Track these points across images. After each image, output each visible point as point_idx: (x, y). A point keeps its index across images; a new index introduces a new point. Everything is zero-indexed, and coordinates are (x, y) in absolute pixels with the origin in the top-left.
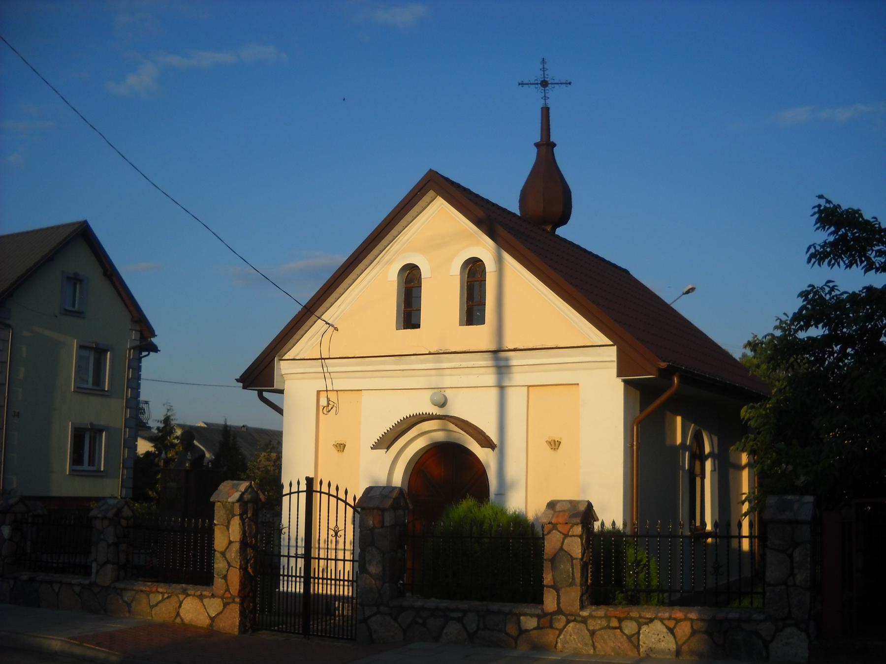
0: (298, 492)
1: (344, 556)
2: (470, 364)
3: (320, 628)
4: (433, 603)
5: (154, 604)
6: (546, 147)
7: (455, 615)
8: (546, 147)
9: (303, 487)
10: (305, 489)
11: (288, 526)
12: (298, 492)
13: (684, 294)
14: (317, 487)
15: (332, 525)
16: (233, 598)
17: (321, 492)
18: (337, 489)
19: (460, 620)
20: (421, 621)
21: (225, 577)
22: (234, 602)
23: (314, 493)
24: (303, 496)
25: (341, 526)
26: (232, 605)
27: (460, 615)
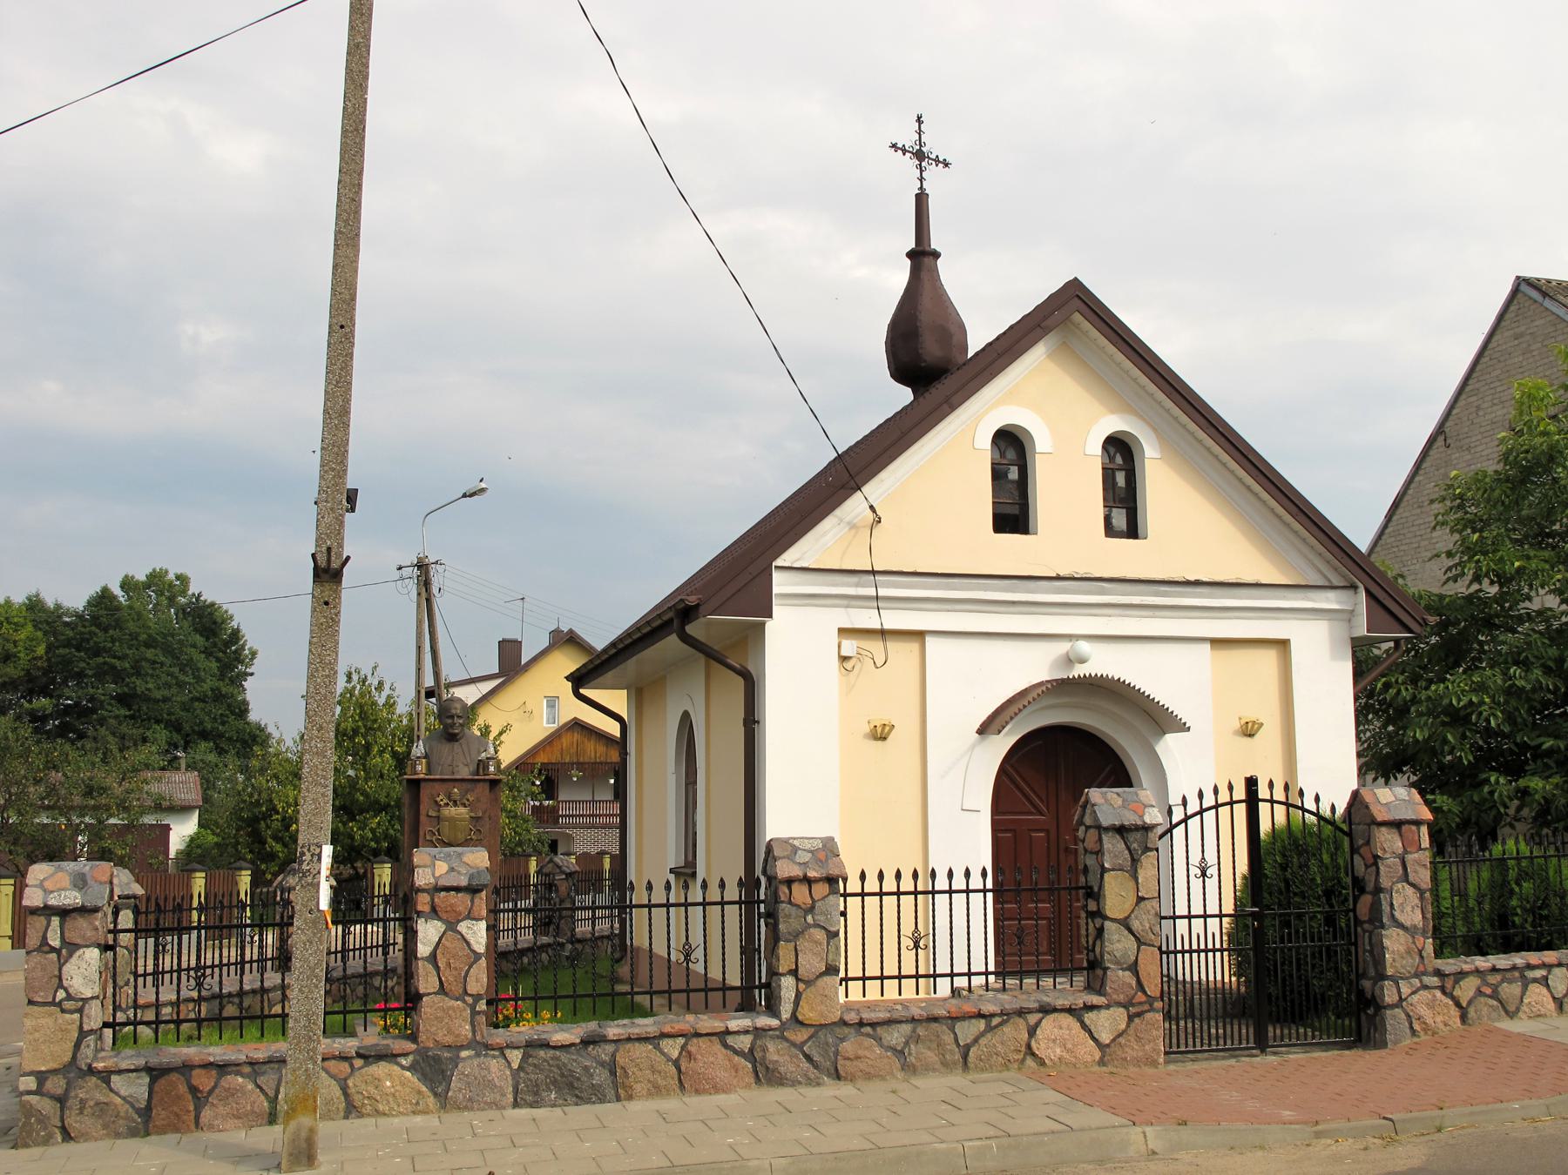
0: (1231, 803)
1: (968, 899)
2: (1136, 600)
3: (1182, 1023)
4: (1502, 961)
5: (969, 1041)
6: (922, 256)
7: (1539, 973)
8: (922, 256)
9: (1240, 794)
10: (1243, 797)
11: (1216, 862)
12: (1231, 803)
13: (465, 496)
14: (1263, 792)
15: (1195, 858)
16: (1151, 1000)
17: (1272, 801)
18: (1317, 799)
19: (1544, 981)
20: (1488, 991)
21: (1134, 968)
22: (1152, 1009)
23: (1260, 803)
24: (1241, 810)
25: (1211, 858)
26: (1148, 1016)
27: (1544, 972)
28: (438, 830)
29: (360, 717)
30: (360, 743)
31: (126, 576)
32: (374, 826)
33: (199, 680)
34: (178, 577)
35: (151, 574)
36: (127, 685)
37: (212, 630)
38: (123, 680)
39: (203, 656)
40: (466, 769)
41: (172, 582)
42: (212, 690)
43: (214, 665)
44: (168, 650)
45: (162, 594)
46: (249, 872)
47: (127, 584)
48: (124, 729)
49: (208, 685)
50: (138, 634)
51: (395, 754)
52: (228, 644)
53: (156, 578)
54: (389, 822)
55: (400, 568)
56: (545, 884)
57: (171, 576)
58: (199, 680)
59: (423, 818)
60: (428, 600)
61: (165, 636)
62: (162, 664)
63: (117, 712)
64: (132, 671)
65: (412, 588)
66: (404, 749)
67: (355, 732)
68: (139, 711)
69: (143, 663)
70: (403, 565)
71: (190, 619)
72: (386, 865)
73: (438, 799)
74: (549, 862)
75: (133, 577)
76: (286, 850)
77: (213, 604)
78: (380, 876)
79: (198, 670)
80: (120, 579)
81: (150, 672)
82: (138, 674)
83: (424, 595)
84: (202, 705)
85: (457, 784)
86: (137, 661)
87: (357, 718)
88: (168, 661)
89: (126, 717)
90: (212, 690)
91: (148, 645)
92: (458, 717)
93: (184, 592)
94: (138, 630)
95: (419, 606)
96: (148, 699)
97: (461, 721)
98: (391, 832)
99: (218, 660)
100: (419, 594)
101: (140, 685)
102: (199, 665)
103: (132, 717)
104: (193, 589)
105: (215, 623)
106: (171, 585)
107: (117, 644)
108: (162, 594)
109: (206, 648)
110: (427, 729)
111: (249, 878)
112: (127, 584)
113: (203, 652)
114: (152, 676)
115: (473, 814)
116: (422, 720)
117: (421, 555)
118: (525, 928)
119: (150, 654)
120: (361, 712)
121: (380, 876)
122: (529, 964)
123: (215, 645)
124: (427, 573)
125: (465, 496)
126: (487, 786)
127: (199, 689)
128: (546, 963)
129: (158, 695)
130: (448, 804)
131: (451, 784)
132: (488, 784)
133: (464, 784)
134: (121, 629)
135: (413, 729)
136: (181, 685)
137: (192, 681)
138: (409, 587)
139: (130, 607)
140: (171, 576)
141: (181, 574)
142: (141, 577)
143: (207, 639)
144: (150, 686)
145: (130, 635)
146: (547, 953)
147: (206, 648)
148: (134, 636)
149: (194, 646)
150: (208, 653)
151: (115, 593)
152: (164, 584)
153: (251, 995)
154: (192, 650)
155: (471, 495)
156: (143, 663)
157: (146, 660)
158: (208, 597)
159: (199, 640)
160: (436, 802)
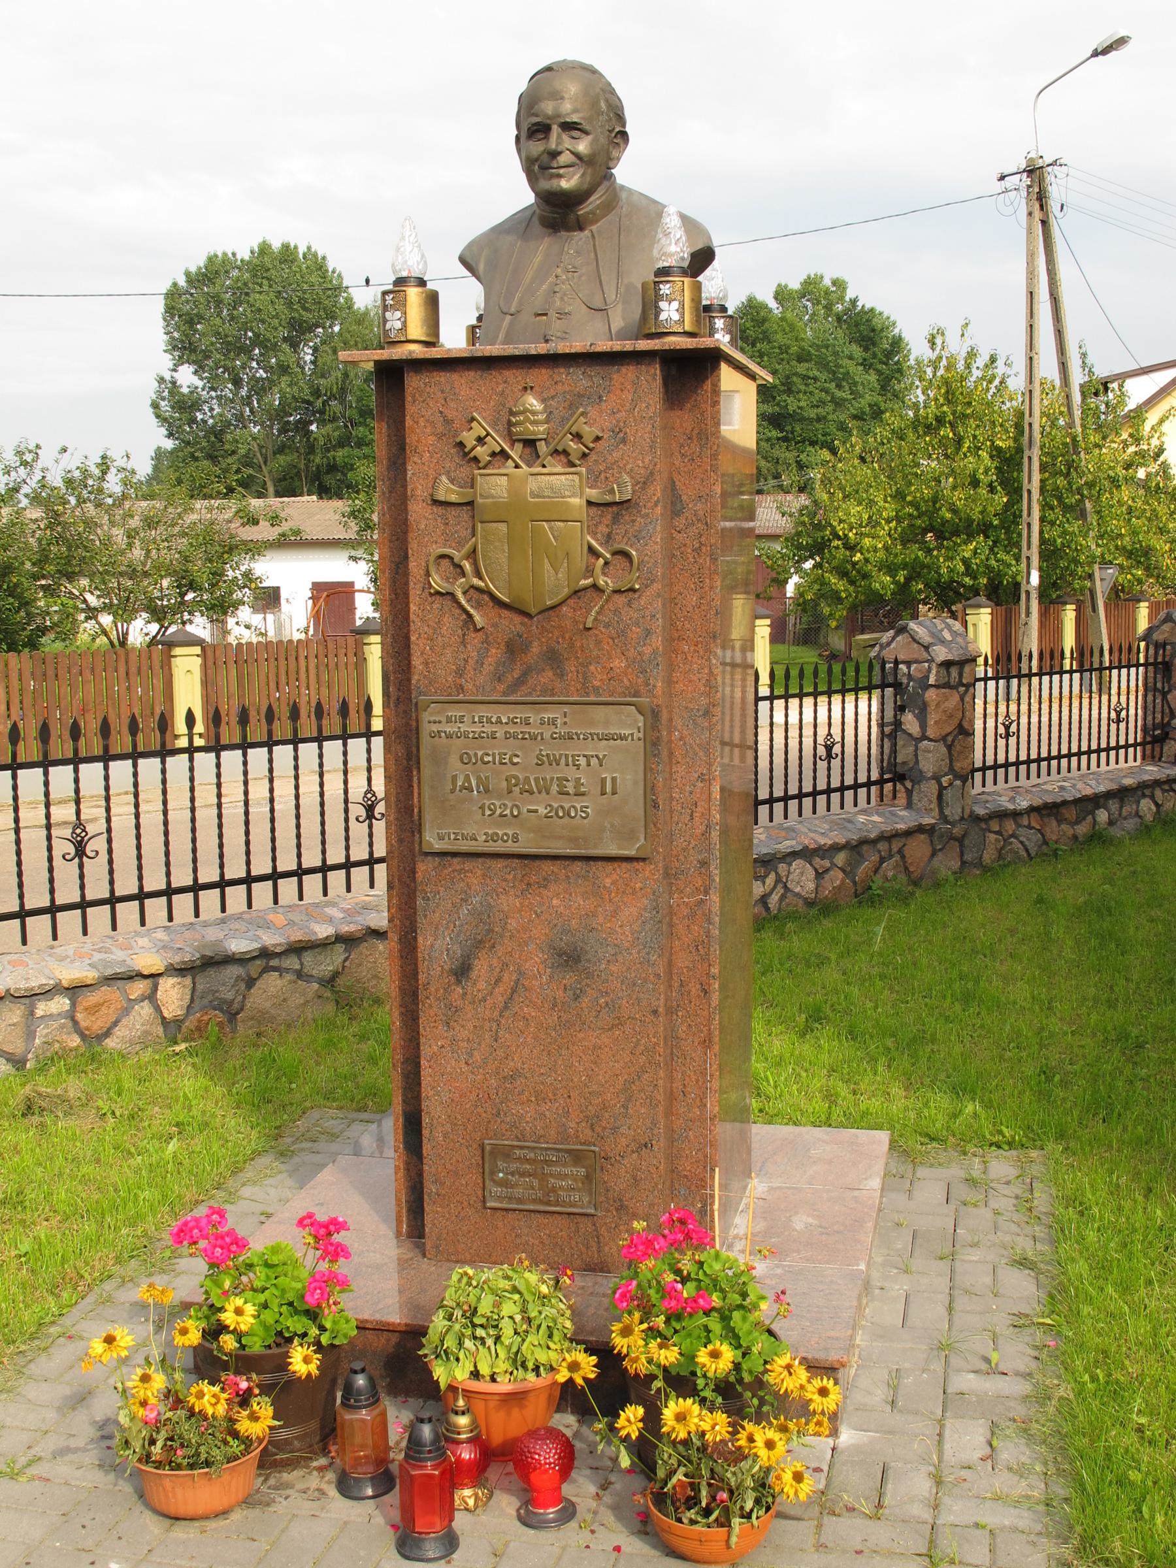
13: (1096, 54)
28: (472, 555)
29: (947, 399)
30: (946, 437)
31: (779, 285)
32: (967, 555)
33: (856, 395)
34: (834, 283)
35: (805, 282)
36: (778, 404)
37: (870, 339)
38: (774, 398)
39: (861, 368)
40: (599, 325)
41: (828, 288)
42: (870, 405)
43: (873, 377)
44: (823, 365)
45: (819, 302)
46: (768, 622)
47: (781, 295)
48: (777, 452)
49: (869, 398)
50: (788, 347)
51: (997, 452)
52: (889, 354)
53: (811, 287)
54: (991, 549)
55: (1002, 178)
56: (1155, 664)
57: (827, 282)
58: (856, 395)
59: (418, 511)
60: (1044, 223)
61: (818, 348)
62: (815, 379)
63: (769, 435)
64: (782, 388)
65: (1019, 203)
66: (1011, 443)
67: (940, 420)
68: (792, 433)
69: (795, 379)
70: (1006, 173)
71: (844, 327)
72: (983, 610)
73: (469, 438)
74: (1165, 621)
75: (786, 286)
76: (851, 589)
77: (872, 310)
78: (974, 625)
79: (855, 384)
80: (773, 289)
81: (803, 388)
82: (789, 391)
83: (1037, 214)
84: (860, 423)
85: (540, 376)
86: (788, 377)
87: (942, 400)
88: (823, 376)
89: (778, 439)
90: (870, 405)
91: (800, 359)
92: (568, 127)
93: (841, 299)
94: (789, 342)
95: (1030, 231)
96: (802, 419)
97: (582, 147)
98: (993, 563)
99: (879, 373)
100: (1030, 214)
101: (792, 404)
102: (857, 379)
103: (785, 439)
104: (850, 294)
105: (873, 330)
106: (827, 293)
107: (766, 358)
108: (819, 302)
109: (865, 360)
110: (1043, 414)
111: (768, 630)
112: (781, 295)
113: (861, 364)
114: (805, 393)
115: (593, 493)
116: (1036, 401)
117: (1033, 155)
118: (1126, 746)
119: (802, 368)
120: (947, 392)
121: (974, 625)
122: (1111, 823)
123: (874, 356)
124: (1041, 182)
125: (1096, 54)
126: (651, 379)
127: (857, 405)
128: (1149, 818)
129: (812, 413)
130: (504, 455)
131: (514, 377)
132: (656, 370)
133: (561, 373)
134: (769, 342)
135: (1023, 414)
136: (838, 404)
137: (850, 397)
138: (1016, 204)
139: (783, 319)
140: (827, 282)
141: (838, 279)
142: (795, 285)
143: (866, 349)
144: (802, 404)
145: (780, 348)
146: (1152, 797)
147: (865, 360)
148: (784, 349)
149: (851, 358)
150: (866, 365)
151: (770, 306)
152: (819, 290)
153: (340, 948)
154: (849, 362)
155: (1105, 51)
156: (795, 379)
157: (796, 374)
158: (866, 301)
159: (856, 350)
160: (461, 445)
